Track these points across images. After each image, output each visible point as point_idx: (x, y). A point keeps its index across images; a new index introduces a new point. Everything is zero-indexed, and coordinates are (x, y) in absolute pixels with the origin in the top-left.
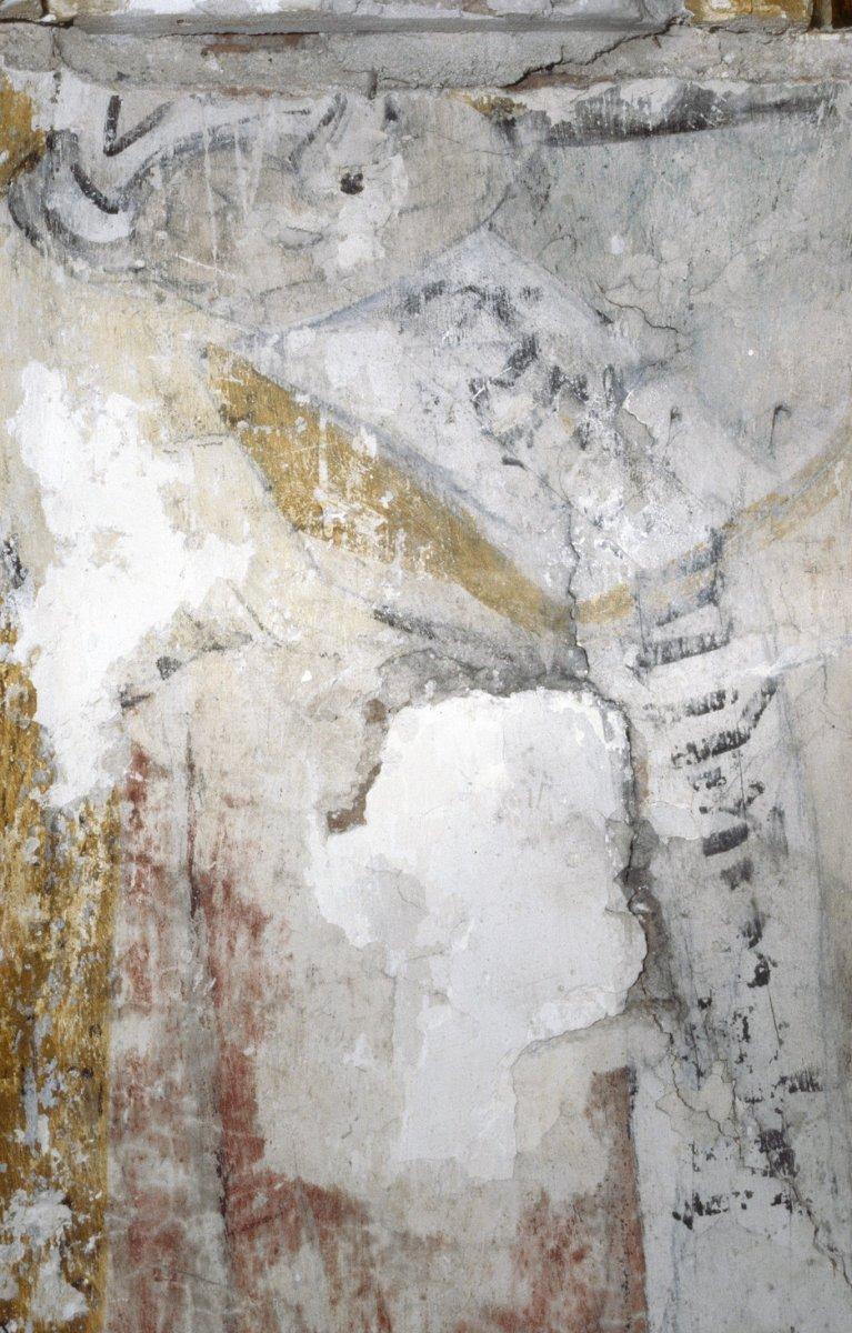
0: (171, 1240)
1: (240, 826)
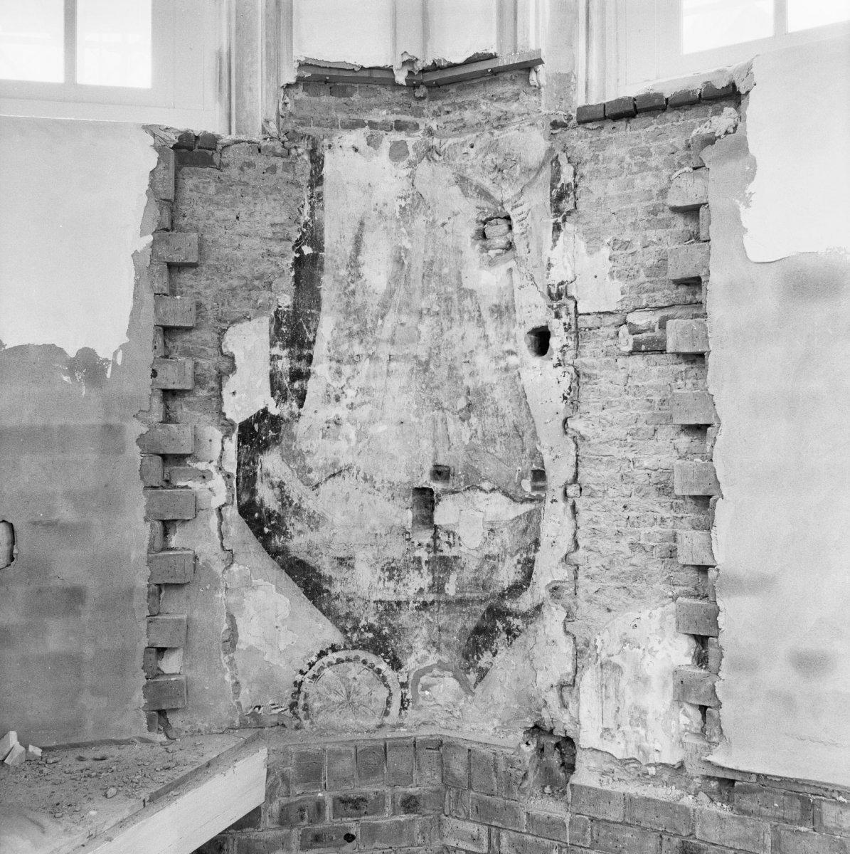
0: (450, 298)
1: (61, 829)
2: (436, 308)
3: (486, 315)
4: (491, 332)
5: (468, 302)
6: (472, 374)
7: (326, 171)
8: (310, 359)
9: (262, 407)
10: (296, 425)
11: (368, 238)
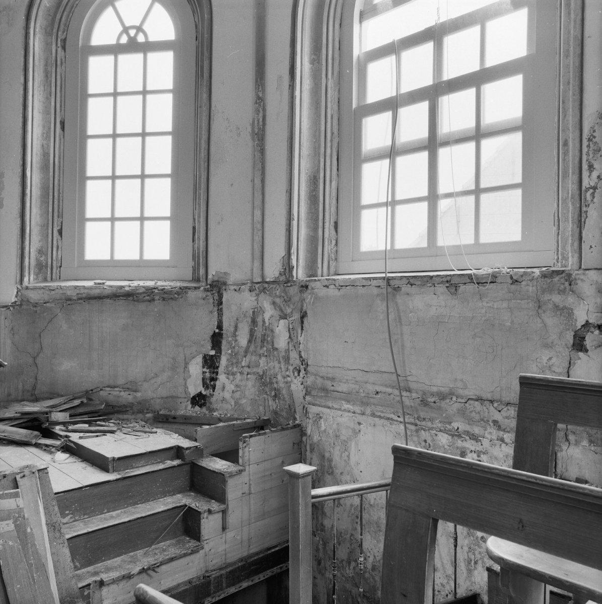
2: (266, 354)
3: (281, 359)
4: (282, 367)
5: (275, 353)
6: (277, 383)
7: (224, 300)
8: (217, 373)
9: (199, 391)
10: (212, 398)
11: (240, 325)
